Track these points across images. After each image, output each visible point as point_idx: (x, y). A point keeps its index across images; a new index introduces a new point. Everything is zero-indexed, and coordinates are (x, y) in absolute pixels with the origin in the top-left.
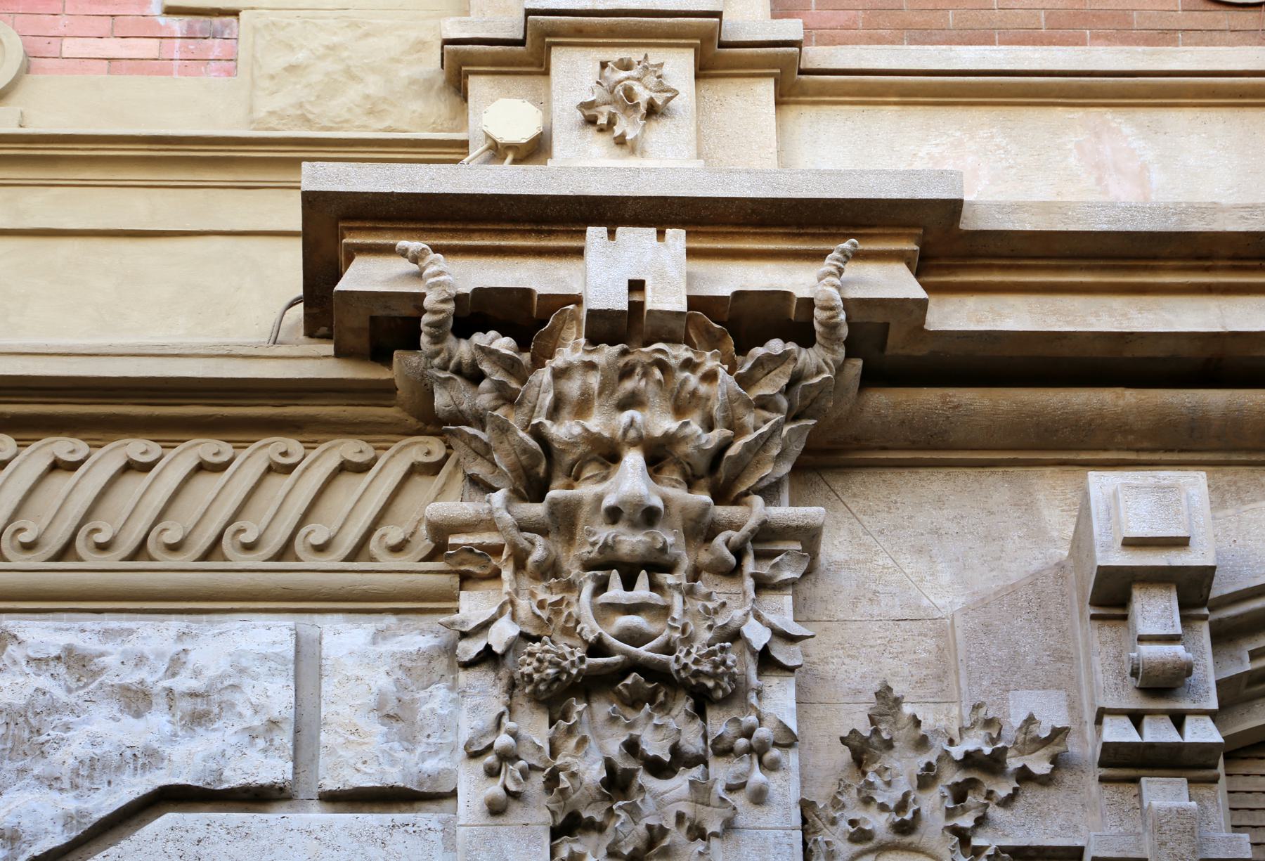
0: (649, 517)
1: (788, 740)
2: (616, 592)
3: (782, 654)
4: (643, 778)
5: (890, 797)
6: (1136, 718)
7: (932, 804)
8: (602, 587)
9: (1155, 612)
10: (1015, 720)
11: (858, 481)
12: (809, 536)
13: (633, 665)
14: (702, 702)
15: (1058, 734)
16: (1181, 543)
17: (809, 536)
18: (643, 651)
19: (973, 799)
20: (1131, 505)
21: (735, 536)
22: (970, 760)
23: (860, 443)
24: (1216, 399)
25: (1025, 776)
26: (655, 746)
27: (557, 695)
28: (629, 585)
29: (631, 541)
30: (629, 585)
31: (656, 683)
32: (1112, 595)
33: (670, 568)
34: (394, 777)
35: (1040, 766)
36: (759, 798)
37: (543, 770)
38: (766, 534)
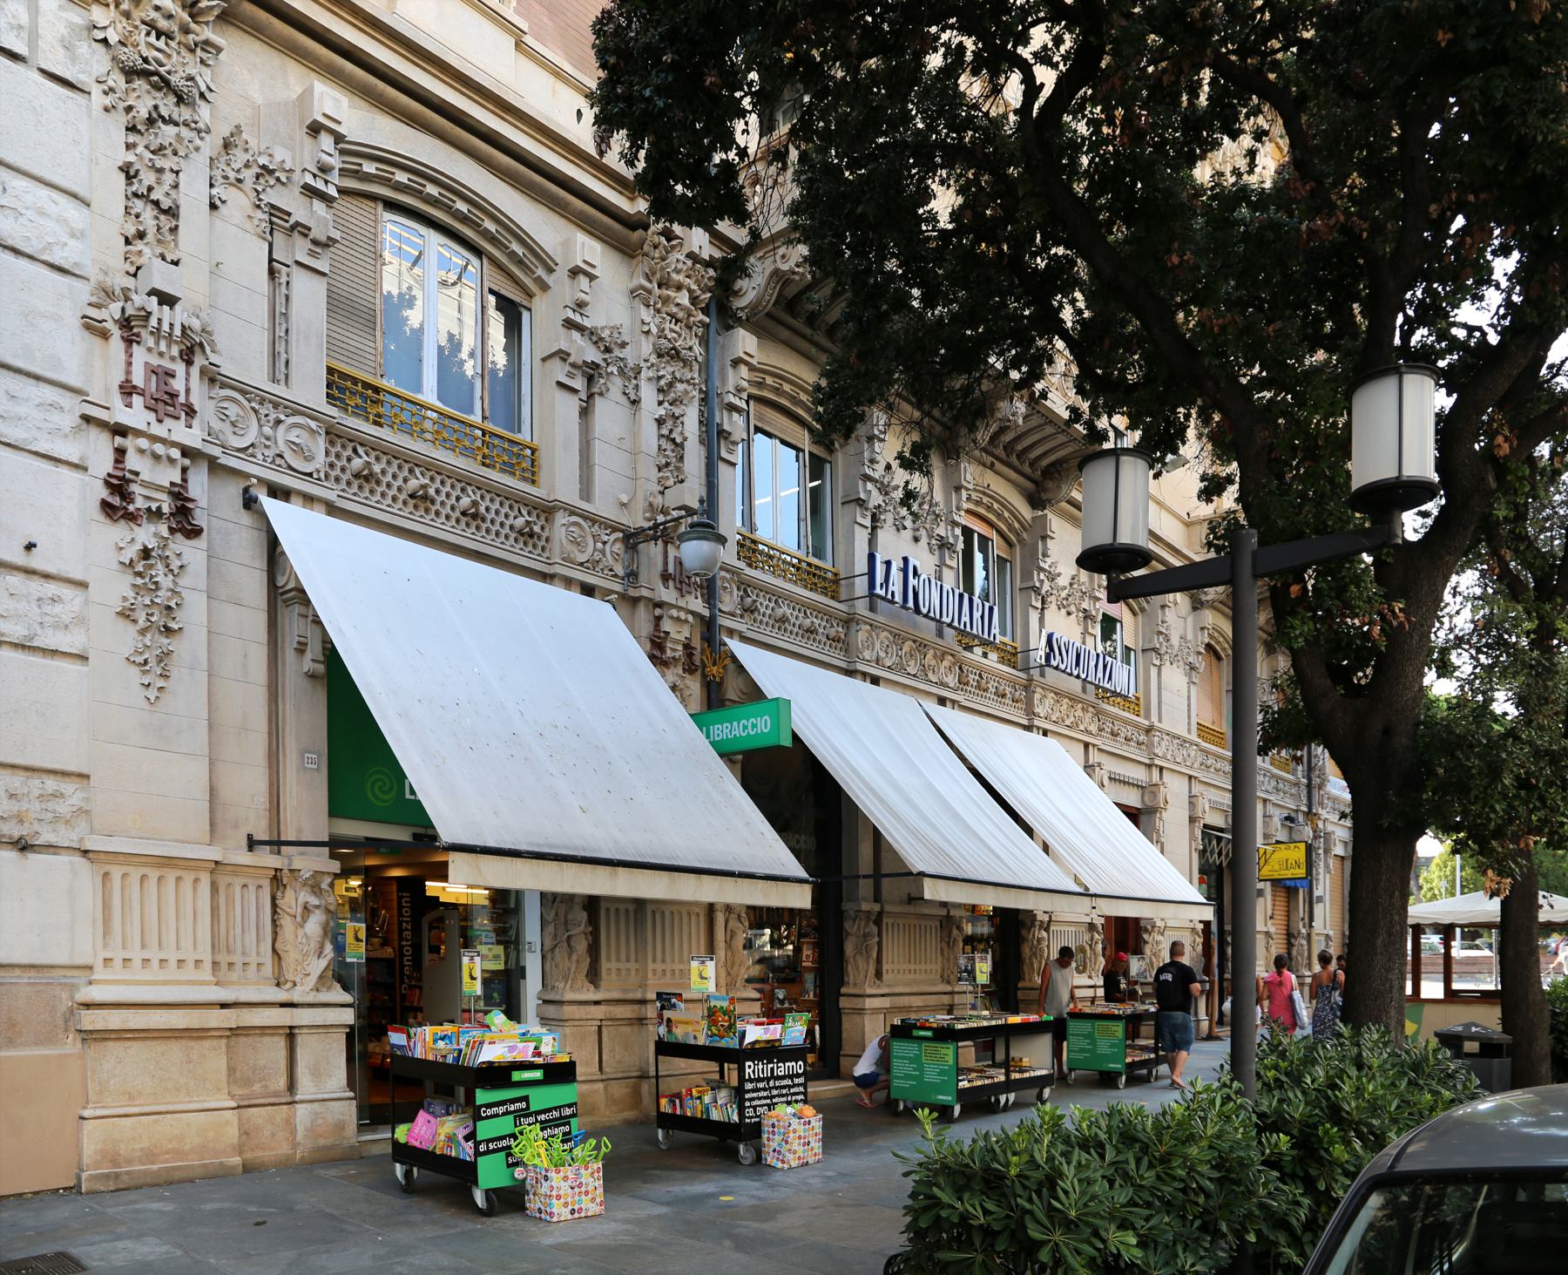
0: (170, 17)
1: (208, 131)
2: (152, 39)
3: (207, 94)
4: (160, 123)
5: (236, 166)
6: (315, 176)
7: (249, 175)
8: (148, 34)
9: (326, 142)
10: (278, 158)
11: (231, 29)
12: (219, 50)
13: (156, 73)
14: (180, 100)
15: (291, 170)
16: (339, 123)
17: (219, 50)
18: (161, 69)
19: (262, 180)
20: (331, 101)
21: (197, 39)
22: (264, 167)
23: (235, 16)
24: (349, 67)
25: (278, 179)
26: (164, 112)
27: (131, 73)
28: (158, 38)
29: (163, 24)
30: (158, 38)
31: (163, 85)
32: (315, 129)
33: (172, 39)
34: (67, 76)
35: (284, 179)
36: (197, 149)
37: (819, 552)
38: (207, 42)
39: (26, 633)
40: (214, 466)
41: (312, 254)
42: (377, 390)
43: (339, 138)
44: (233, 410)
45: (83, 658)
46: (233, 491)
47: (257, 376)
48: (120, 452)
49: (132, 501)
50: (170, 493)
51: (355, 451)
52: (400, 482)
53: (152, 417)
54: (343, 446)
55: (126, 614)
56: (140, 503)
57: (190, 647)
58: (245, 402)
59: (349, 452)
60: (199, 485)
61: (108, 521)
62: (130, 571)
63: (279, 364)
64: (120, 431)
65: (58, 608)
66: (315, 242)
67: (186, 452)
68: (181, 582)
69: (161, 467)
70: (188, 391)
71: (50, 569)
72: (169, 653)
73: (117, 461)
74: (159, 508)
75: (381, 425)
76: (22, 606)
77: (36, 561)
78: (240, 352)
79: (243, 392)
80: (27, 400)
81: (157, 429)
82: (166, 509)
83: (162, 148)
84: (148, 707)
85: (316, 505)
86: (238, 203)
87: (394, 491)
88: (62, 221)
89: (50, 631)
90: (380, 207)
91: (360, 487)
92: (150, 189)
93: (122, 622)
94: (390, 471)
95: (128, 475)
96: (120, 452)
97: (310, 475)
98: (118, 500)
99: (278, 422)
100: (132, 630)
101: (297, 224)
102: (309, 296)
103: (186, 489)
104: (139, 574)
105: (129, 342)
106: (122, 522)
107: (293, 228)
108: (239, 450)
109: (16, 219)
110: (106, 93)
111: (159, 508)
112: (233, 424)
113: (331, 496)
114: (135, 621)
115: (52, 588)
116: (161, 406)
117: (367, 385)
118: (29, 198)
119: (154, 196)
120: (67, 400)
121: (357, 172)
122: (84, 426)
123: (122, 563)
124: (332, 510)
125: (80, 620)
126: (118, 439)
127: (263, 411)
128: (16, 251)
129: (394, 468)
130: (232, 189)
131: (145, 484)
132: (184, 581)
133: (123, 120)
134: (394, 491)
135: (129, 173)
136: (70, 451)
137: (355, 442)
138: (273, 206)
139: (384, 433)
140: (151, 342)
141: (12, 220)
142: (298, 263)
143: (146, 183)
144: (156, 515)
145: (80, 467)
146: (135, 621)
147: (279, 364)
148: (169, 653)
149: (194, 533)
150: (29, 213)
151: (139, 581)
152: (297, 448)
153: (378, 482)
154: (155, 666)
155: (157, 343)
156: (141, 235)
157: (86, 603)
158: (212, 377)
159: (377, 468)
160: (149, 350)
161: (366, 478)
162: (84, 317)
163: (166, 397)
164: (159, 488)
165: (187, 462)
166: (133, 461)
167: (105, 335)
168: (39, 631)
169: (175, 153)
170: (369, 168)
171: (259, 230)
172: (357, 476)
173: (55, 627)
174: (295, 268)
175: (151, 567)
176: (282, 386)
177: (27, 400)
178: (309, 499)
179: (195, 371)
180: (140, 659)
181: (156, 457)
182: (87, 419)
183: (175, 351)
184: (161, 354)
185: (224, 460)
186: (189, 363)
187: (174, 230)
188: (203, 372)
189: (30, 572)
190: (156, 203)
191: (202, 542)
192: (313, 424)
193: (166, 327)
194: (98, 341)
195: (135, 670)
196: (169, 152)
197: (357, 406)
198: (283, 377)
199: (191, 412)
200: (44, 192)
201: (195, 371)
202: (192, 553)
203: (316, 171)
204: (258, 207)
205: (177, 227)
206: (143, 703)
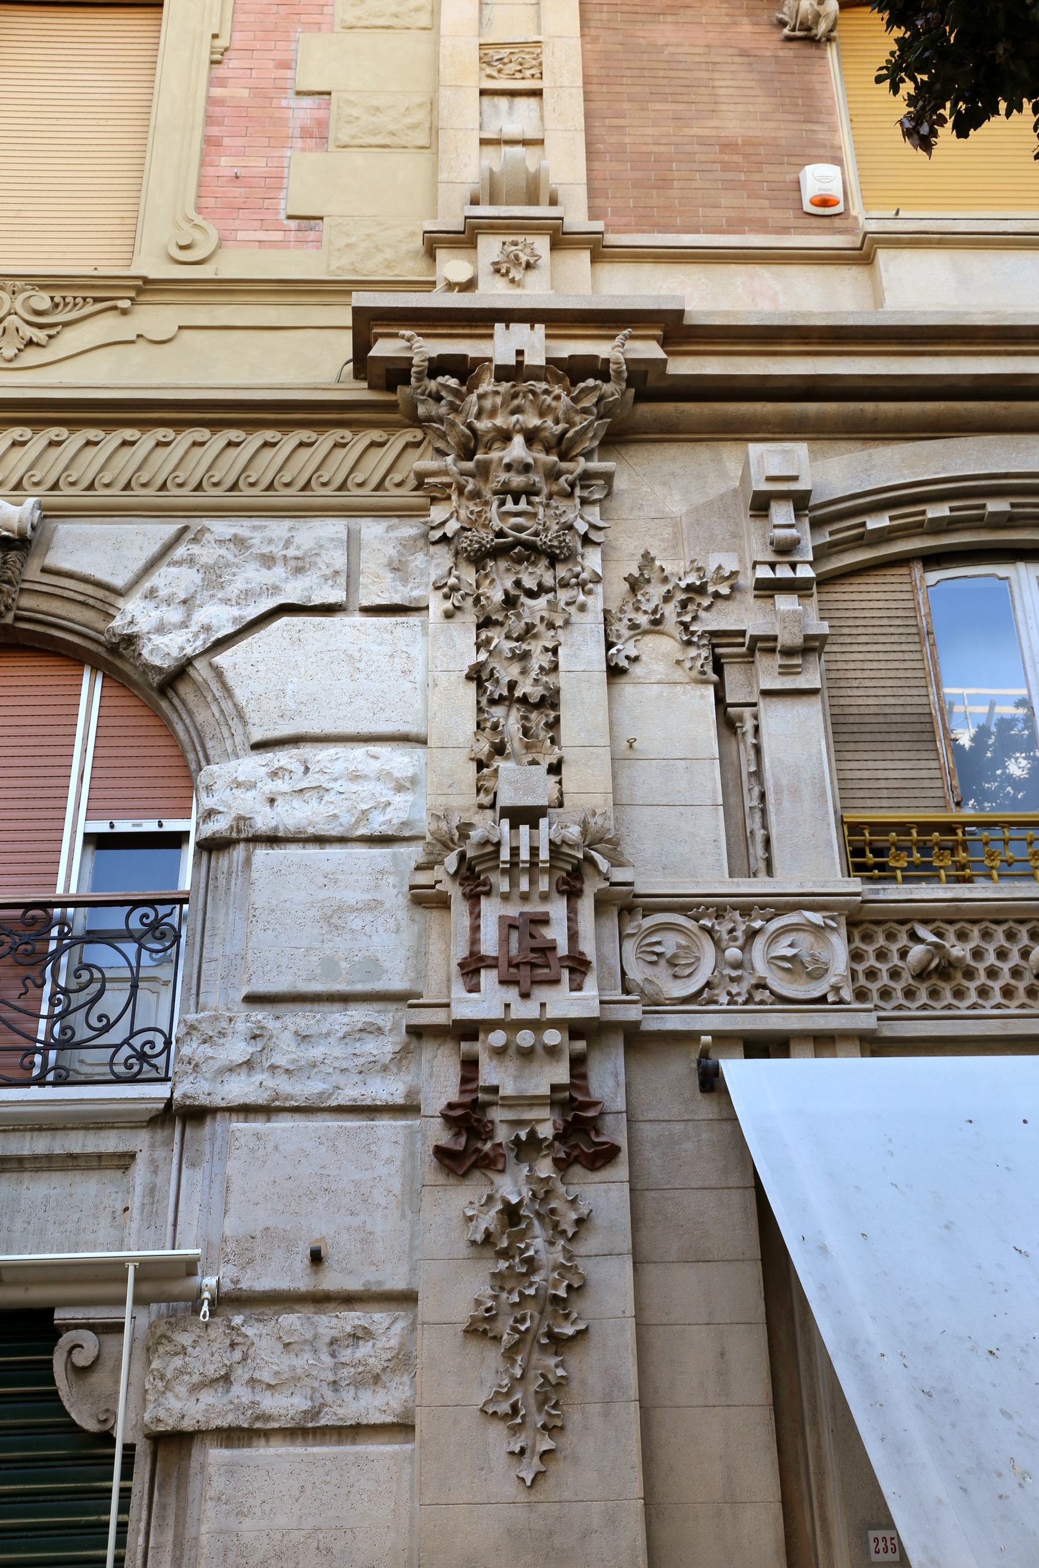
0: (526, 468)
2: (510, 506)
3: (594, 536)
4: (523, 599)
5: (649, 607)
7: (670, 610)
8: (502, 503)
9: (782, 513)
11: (633, 449)
12: (608, 477)
13: (518, 542)
15: (734, 574)
16: (795, 479)
17: (608, 477)
21: (570, 477)
22: (689, 588)
23: (634, 430)
25: (717, 595)
26: (529, 583)
27: (479, 558)
28: (516, 502)
29: (517, 480)
33: (537, 494)
35: (724, 590)
36: (582, 608)
39: (305, 1405)
40: (636, 1040)
41: (786, 671)
42: (948, 828)
43: (800, 501)
44: (670, 943)
45: (402, 1428)
46: (681, 1069)
47: (713, 877)
48: (470, 1066)
49: (490, 1135)
50: (553, 1104)
51: (914, 937)
52: (1015, 959)
53: (512, 994)
54: (891, 937)
55: (479, 1329)
56: (503, 1135)
57: (609, 1356)
58: (690, 924)
59: (903, 940)
60: (608, 1079)
61: (452, 1181)
62: (489, 1253)
63: (750, 841)
64: (468, 1031)
65: (364, 1350)
66: (789, 652)
67: (576, 1029)
68: (582, 1248)
69: (535, 1066)
70: (573, 936)
71: (353, 1285)
72: (561, 1384)
73: (465, 1081)
74: (532, 1134)
75: (969, 880)
76: (302, 1361)
77: (332, 1281)
78: (679, 848)
79: (682, 909)
80: (328, 1035)
81: (527, 1010)
82: (546, 1131)
83: (529, 628)
84: (522, 1497)
85: (840, 1047)
86: (658, 655)
87: (1006, 978)
88: (383, 776)
89: (348, 1394)
90: (917, 570)
91: (934, 994)
92: (512, 686)
93: (474, 1347)
94: (991, 949)
95: (482, 1096)
96: (470, 1066)
97: (823, 999)
98: (467, 1143)
99: (752, 934)
100: (493, 1356)
101: (755, 639)
102: (794, 737)
103: (585, 1091)
104: (505, 1254)
105: (473, 898)
106: (477, 1174)
107: (752, 651)
108: (685, 1000)
109: (321, 798)
110: (447, 597)
111: (532, 1134)
112: (672, 963)
113: (866, 1021)
114: (497, 1339)
115: (353, 1318)
116: (525, 972)
117: (925, 828)
118: (338, 767)
119: (518, 693)
120: (387, 1017)
121: (860, 537)
122: (414, 1043)
123: (473, 1243)
124: (874, 1045)
125: (402, 1361)
126: (465, 1046)
127: (722, 929)
128: (321, 840)
129: (1000, 938)
130: (648, 638)
131: (510, 1103)
132: (590, 1245)
133: (470, 617)
134: (1006, 978)
135: (477, 676)
136: (388, 1089)
137: (905, 920)
138: (714, 634)
139: (980, 890)
140: (504, 885)
141: (314, 803)
142: (766, 693)
143: (505, 680)
144: (528, 1147)
145: (408, 1109)
146: (497, 1339)
147: (750, 841)
148: (561, 1384)
149: (604, 1156)
150: (336, 786)
151: (503, 1265)
152: (792, 966)
153: (969, 974)
154: (536, 1413)
155: (514, 884)
156: (499, 750)
157: (413, 1328)
158: (624, 906)
159: (959, 951)
160: (505, 897)
161: (941, 971)
162: (412, 887)
163: (532, 957)
164: (534, 1101)
165: (581, 1045)
166: (490, 1073)
167: (443, 903)
168: (329, 1395)
169: (551, 626)
170: (876, 522)
171: (694, 673)
172: (922, 975)
173: (358, 1383)
174: (762, 703)
175: (522, 1235)
176: (763, 877)
177: (328, 1035)
178: (824, 1042)
179: (586, 906)
180: (504, 1407)
181: (527, 1054)
182: (416, 1032)
183: (544, 884)
184: (525, 897)
185: (653, 1024)
186: (573, 894)
187: (554, 725)
188: (601, 904)
189: (320, 1300)
190: (524, 700)
191: (620, 1171)
192: (816, 918)
193: (525, 855)
194: (435, 915)
195: (497, 1431)
196: (541, 628)
197: (912, 866)
198: (762, 865)
199: (578, 966)
200: (359, 751)
201: (586, 906)
202: (604, 1195)
203: (772, 558)
204: (689, 643)
205: (557, 719)
206: (511, 1490)
